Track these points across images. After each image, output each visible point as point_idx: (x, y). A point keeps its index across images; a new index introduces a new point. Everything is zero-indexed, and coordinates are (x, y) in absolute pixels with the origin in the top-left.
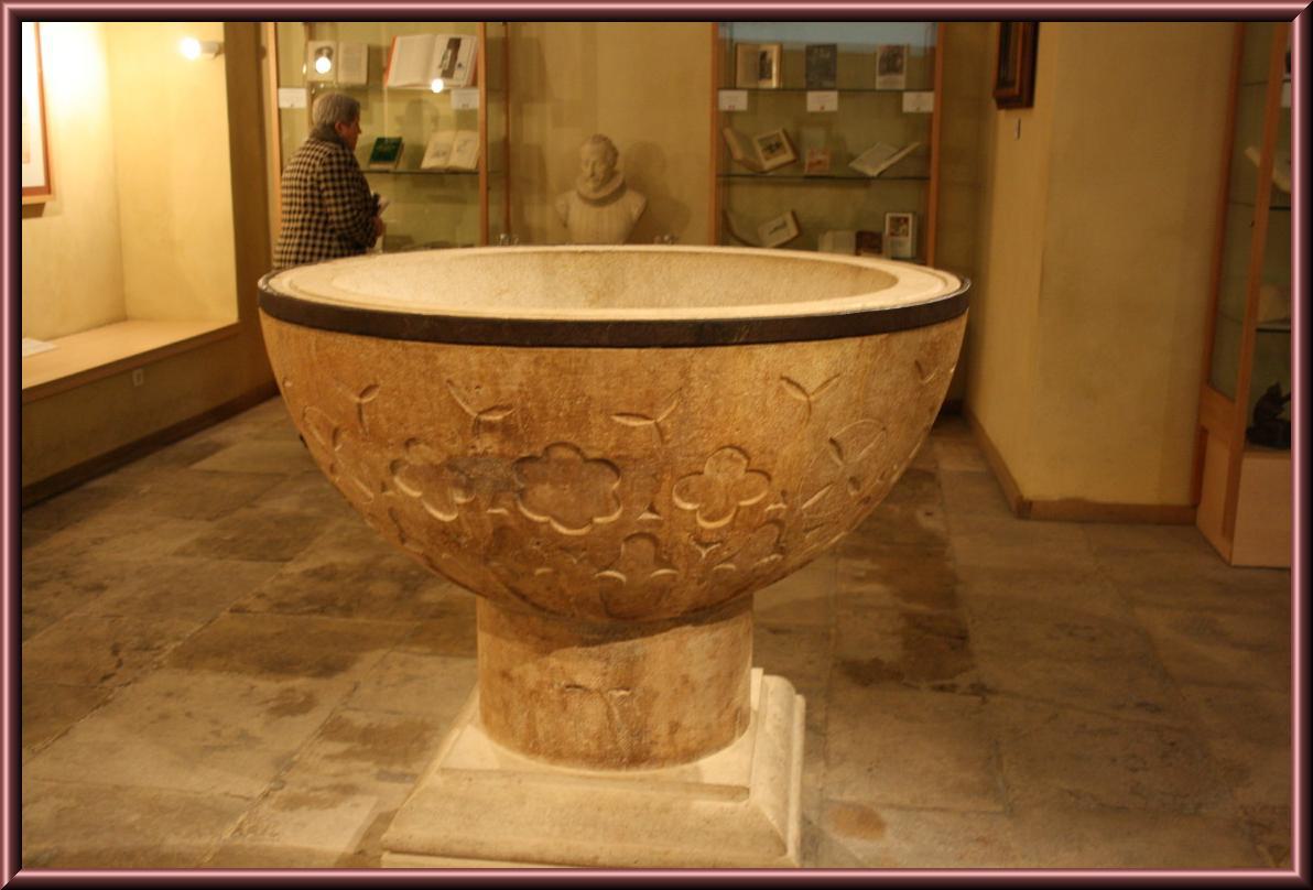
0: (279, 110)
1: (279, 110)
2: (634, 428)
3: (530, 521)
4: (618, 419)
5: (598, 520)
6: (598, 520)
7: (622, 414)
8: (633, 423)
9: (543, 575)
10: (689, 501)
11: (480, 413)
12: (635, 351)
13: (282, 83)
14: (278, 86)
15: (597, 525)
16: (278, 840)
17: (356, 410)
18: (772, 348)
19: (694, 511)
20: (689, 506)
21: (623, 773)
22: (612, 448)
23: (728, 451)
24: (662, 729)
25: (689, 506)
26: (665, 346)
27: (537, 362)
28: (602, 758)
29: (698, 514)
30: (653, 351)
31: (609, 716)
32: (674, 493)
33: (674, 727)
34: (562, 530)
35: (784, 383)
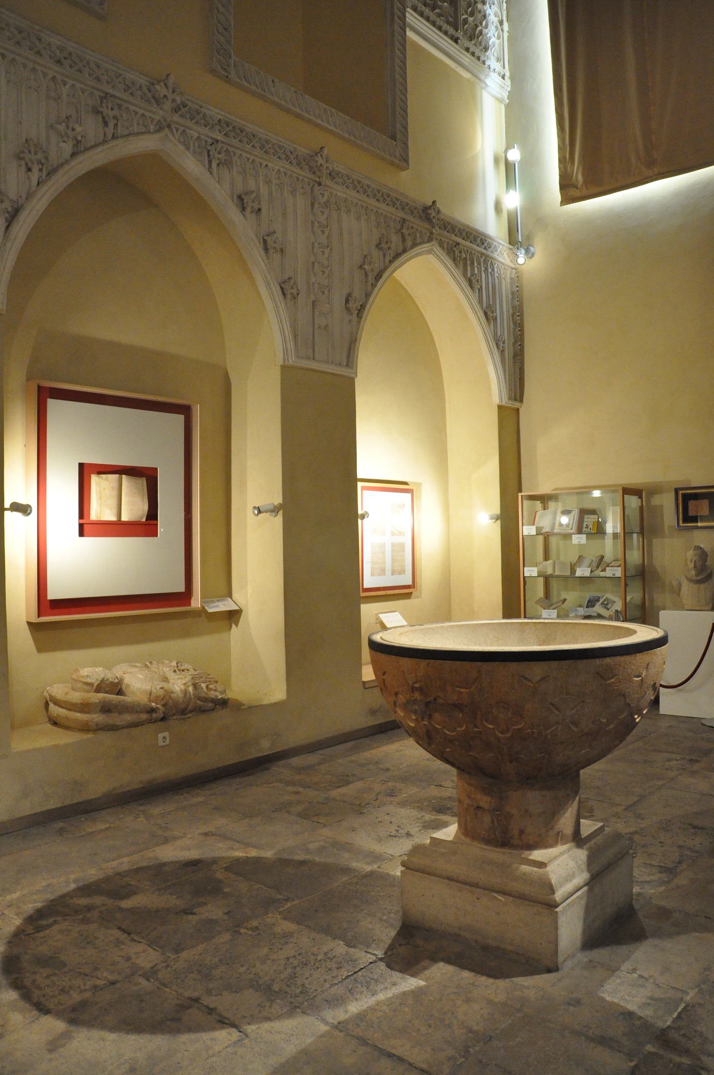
0: (524, 577)
1: (524, 577)
2: (463, 692)
3: (435, 727)
4: (456, 688)
5: (458, 729)
6: (458, 729)
7: (458, 687)
8: (462, 690)
9: (448, 751)
10: (491, 724)
11: (414, 683)
12: (459, 662)
13: (526, 565)
14: (524, 566)
15: (459, 731)
16: (88, 717)
17: (382, 680)
18: (514, 663)
19: (494, 729)
20: (491, 726)
21: (498, 850)
22: (456, 700)
23: (502, 704)
24: (516, 832)
25: (491, 726)
26: (471, 661)
27: (428, 665)
28: (489, 842)
29: (496, 730)
30: (466, 662)
31: (493, 822)
32: (483, 720)
33: (522, 832)
34: (448, 733)
35: (522, 678)
